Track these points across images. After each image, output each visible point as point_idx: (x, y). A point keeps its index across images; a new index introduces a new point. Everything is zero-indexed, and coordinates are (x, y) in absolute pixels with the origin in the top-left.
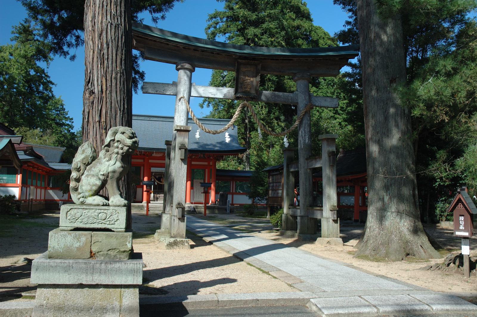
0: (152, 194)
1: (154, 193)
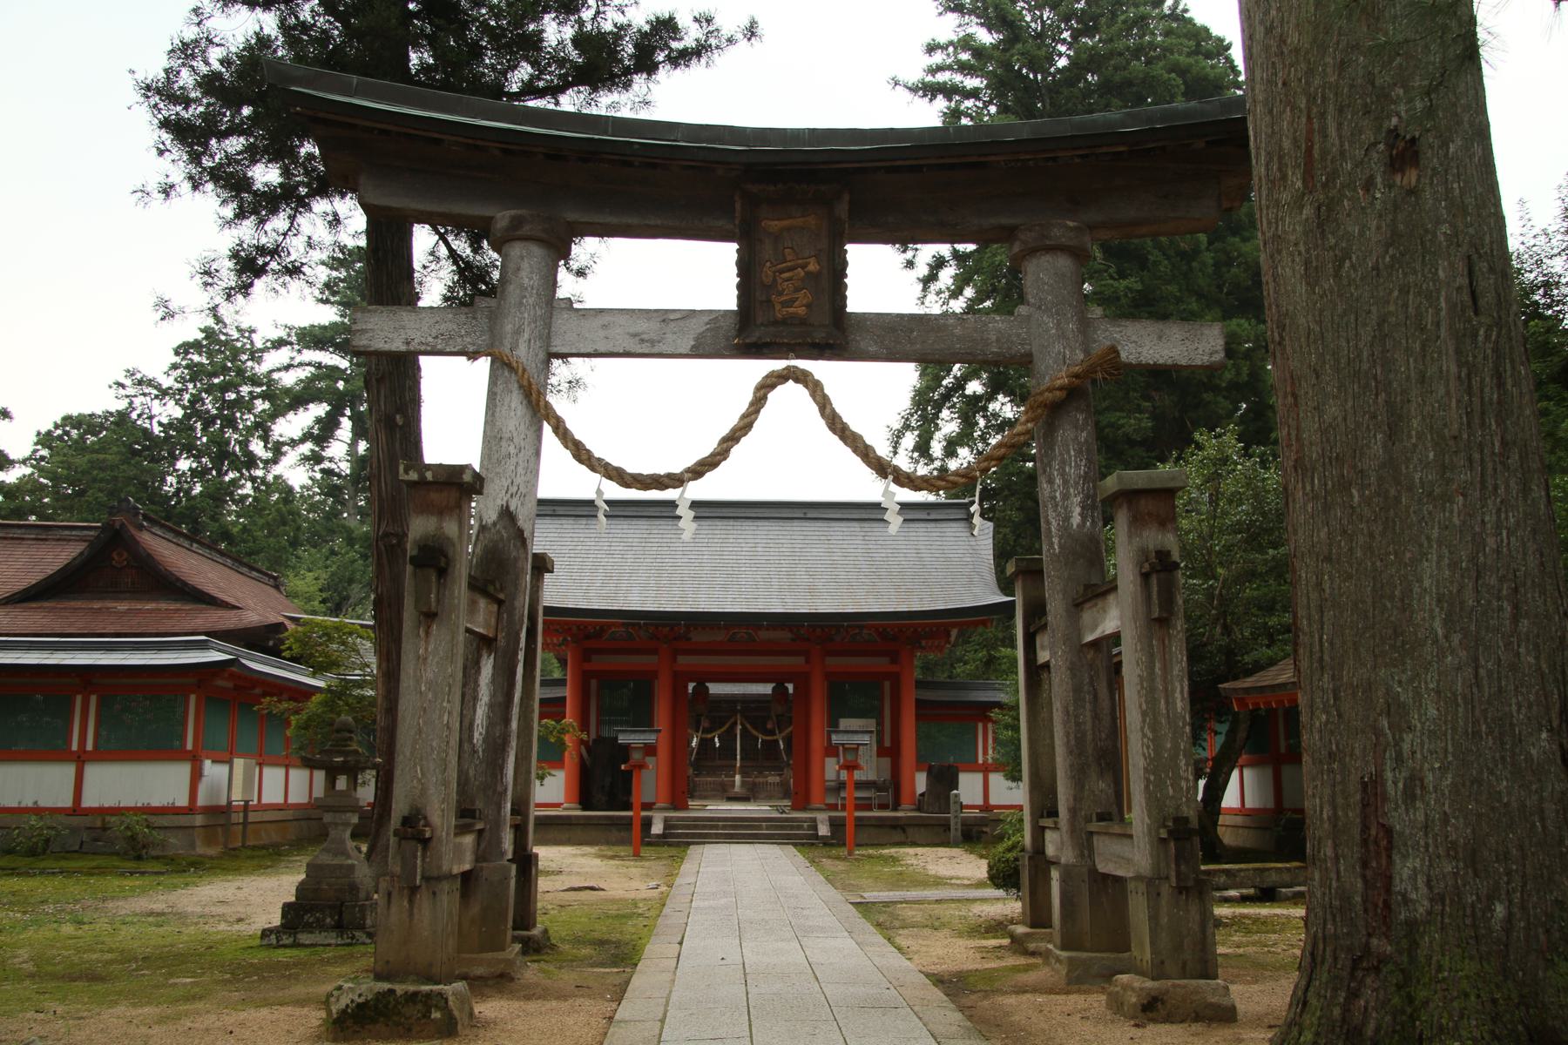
0: (738, 777)
1: (744, 774)
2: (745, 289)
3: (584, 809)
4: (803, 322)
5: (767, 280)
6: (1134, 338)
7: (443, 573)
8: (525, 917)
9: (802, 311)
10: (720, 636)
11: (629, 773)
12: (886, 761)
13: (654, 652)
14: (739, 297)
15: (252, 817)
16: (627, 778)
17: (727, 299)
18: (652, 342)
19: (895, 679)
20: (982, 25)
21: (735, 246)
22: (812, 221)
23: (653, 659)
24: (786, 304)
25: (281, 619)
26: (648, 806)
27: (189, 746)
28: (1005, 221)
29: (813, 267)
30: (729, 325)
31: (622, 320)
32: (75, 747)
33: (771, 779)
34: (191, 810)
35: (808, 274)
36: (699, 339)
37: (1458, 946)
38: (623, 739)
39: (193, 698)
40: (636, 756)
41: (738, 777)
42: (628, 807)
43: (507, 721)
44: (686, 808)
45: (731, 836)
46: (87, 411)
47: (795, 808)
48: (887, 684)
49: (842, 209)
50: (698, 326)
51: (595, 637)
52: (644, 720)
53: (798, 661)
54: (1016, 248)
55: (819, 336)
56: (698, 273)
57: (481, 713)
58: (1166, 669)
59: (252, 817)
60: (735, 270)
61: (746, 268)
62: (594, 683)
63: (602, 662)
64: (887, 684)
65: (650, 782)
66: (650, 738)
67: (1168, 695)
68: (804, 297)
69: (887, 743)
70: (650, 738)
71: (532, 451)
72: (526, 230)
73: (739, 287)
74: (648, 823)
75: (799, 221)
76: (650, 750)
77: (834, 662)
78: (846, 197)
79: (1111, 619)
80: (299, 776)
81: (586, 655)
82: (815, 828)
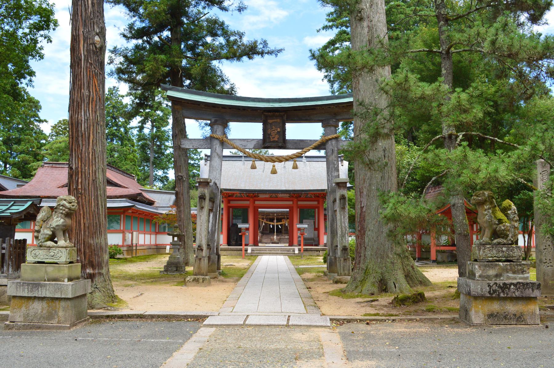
0: (275, 237)
1: (277, 235)
2: (264, 135)
3: (229, 246)
4: (277, 142)
7: (204, 199)
8: (219, 268)
9: (277, 139)
10: (267, 196)
11: (241, 236)
12: (316, 232)
13: (248, 200)
15: (138, 248)
16: (241, 237)
17: (260, 137)
19: (318, 208)
21: (262, 124)
22: (278, 120)
23: (248, 203)
24: (273, 138)
25: (140, 192)
26: (246, 245)
27: (122, 229)
29: (279, 130)
30: (261, 142)
31: (238, 141)
33: (286, 237)
34: (123, 246)
38: (240, 226)
39: (122, 215)
40: (243, 231)
41: (275, 237)
42: (241, 245)
43: (215, 226)
44: (258, 246)
45: (270, 253)
46: (36, 98)
47: (289, 246)
48: (317, 210)
49: (285, 118)
50: (254, 143)
51: (230, 195)
52: (245, 221)
53: (291, 203)
55: (280, 145)
56: (254, 131)
57: (210, 224)
58: (344, 217)
59: (138, 248)
61: (265, 130)
62: (231, 209)
63: (233, 203)
64: (317, 210)
65: (249, 236)
66: (247, 226)
67: (345, 224)
68: (277, 136)
69: (317, 227)
70: (247, 226)
72: (218, 123)
74: (246, 250)
75: (275, 120)
76: (247, 229)
77: (300, 203)
80: (148, 236)
81: (229, 202)
82: (294, 251)
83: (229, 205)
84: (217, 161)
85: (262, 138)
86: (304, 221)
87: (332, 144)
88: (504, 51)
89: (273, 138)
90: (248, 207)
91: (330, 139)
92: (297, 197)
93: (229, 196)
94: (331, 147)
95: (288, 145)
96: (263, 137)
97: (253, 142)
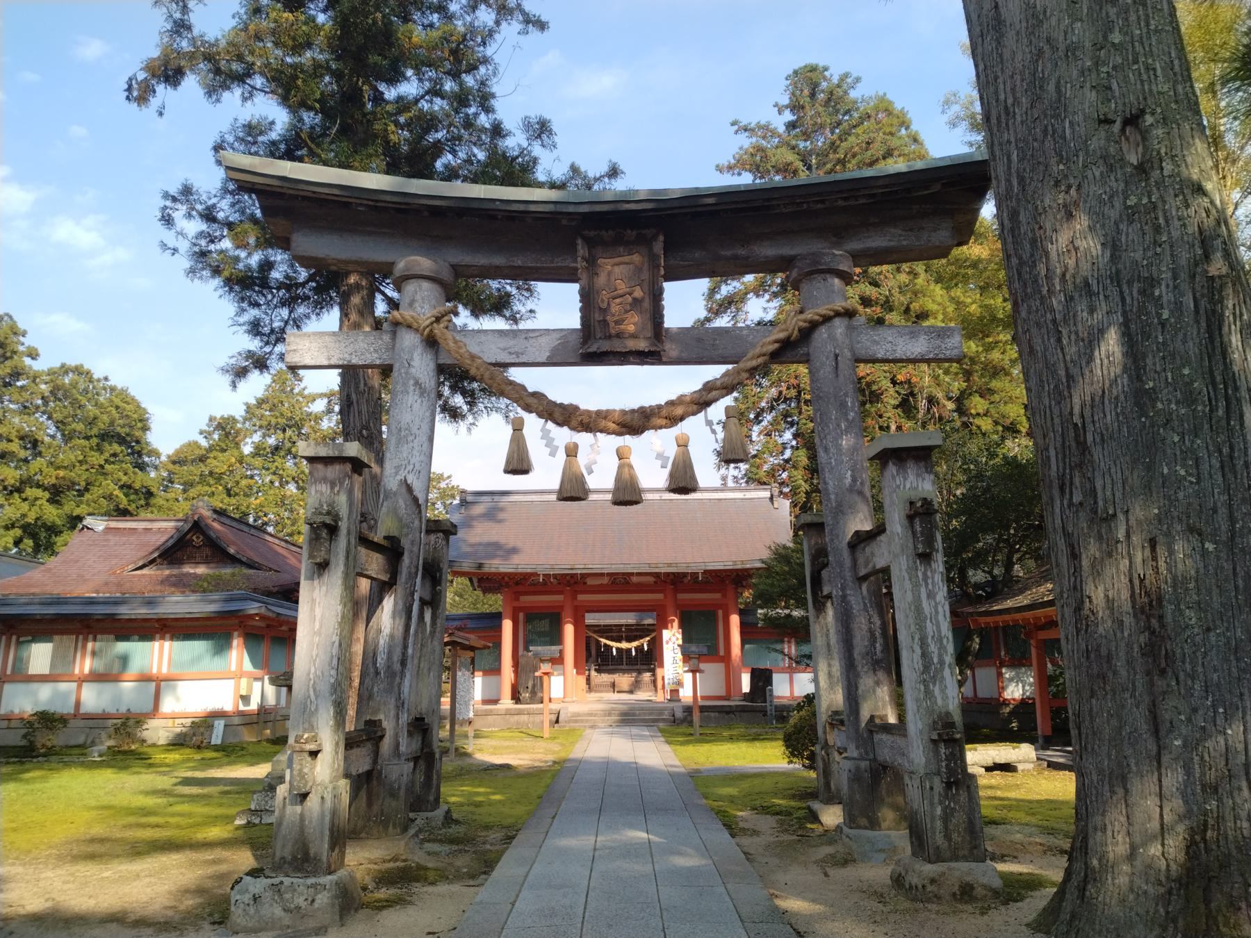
5: (604, 305)
6: (890, 339)
13: (561, 593)
14: (582, 318)
18: (518, 354)
20: (789, 337)
22: (636, 258)
23: (560, 598)
28: (787, 251)
30: (575, 340)
32: (233, 668)
35: (635, 299)
36: (554, 351)
37: (284, 431)
49: (658, 247)
50: (552, 341)
54: (794, 274)
55: (642, 345)
60: (578, 297)
61: (587, 299)
71: (425, 438)
73: (581, 310)
77: (681, 596)
78: (661, 238)
79: (1138, 32)
83: (516, 604)
84: (416, 406)
85: (578, 326)
86: (99, 637)
87: (832, 338)
88: (280, 919)
89: (617, 323)
90: (562, 607)
91: (827, 319)
92: (673, 583)
93: (517, 584)
94: (830, 347)
95: (671, 349)
96: (582, 325)
97: (543, 340)
